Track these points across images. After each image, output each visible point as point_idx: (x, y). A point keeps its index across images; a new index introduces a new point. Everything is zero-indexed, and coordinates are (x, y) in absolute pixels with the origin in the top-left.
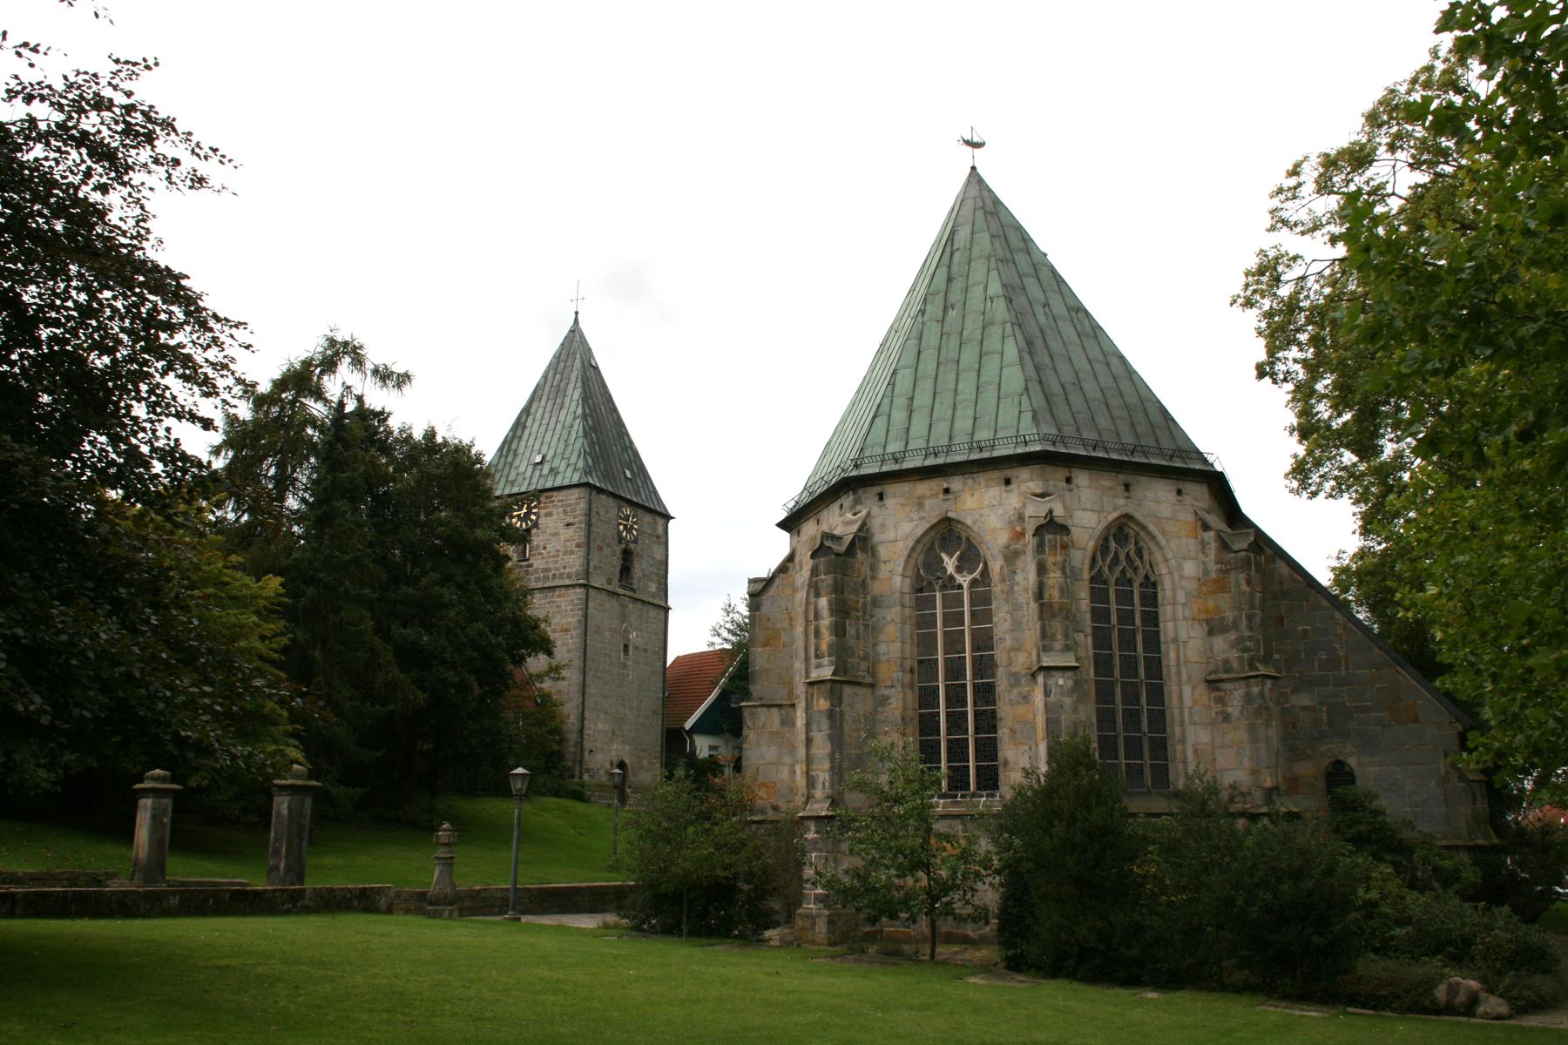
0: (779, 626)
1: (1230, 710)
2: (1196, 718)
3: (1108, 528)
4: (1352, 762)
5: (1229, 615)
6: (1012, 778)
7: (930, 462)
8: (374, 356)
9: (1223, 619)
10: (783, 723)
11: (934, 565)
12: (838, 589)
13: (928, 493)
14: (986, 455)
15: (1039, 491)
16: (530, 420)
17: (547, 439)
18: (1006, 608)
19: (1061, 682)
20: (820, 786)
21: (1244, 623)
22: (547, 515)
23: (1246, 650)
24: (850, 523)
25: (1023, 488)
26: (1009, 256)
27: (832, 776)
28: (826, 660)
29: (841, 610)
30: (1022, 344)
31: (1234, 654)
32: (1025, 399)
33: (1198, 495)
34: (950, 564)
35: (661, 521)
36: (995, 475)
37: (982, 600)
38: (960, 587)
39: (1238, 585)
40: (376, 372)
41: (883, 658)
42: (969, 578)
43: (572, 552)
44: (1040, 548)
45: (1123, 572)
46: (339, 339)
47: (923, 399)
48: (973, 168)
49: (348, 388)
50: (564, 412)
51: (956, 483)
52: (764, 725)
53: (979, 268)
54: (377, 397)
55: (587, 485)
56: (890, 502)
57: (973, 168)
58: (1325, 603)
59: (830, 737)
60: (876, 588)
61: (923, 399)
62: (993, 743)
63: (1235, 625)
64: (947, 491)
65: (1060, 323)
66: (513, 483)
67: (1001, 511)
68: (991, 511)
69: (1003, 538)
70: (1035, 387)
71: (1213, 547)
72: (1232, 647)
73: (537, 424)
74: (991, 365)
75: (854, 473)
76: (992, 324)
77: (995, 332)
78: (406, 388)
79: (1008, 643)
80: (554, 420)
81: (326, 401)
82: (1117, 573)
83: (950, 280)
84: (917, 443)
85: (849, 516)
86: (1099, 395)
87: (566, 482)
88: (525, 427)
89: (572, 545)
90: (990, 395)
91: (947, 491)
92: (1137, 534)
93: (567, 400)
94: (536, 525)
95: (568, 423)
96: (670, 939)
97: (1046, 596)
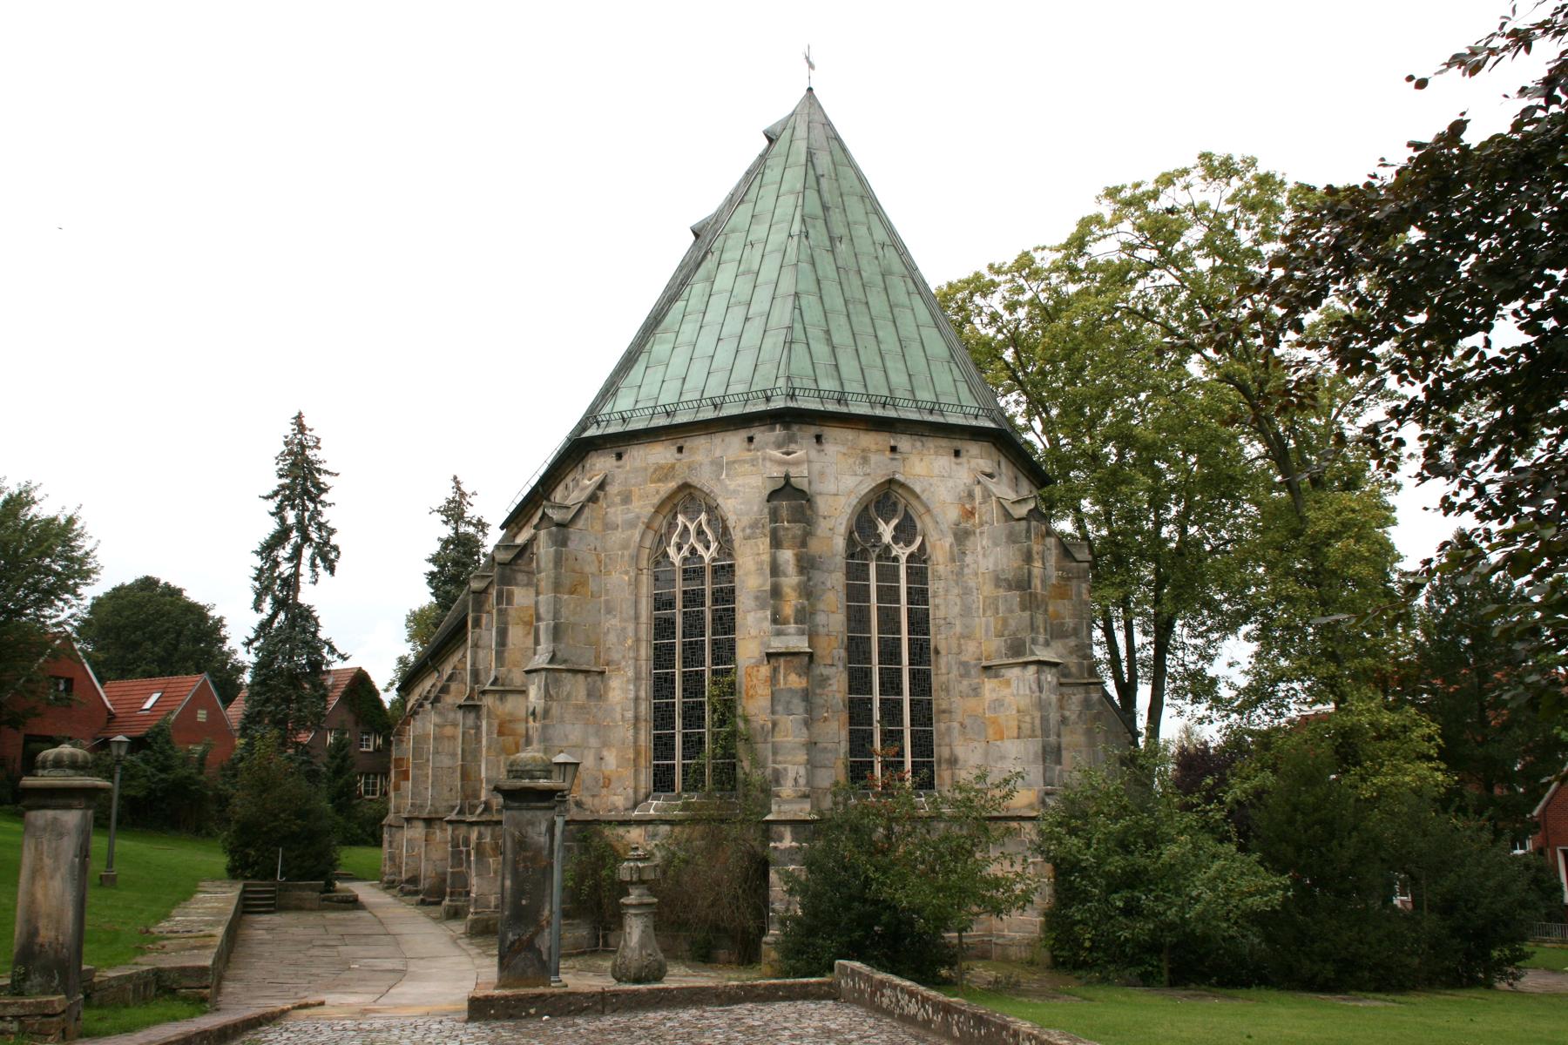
0: (588, 569)
1: (1067, 713)
9: (1062, 624)
10: (589, 695)
13: (873, 447)
15: (988, 470)
18: (956, 591)
20: (790, 782)
25: (974, 462)
34: (887, 531)
36: (944, 443)
37: (918, 574)
39: (1079, 594)
41: (822, 630)
42: (908, 551)
48: (810, 90)
51: (904, 443)
52: (569, 695)
56: (831, 448)
57: (810, 90)
61: (841, 336)
67: (950, 483)
69: (953, 514)
72: (1071, 653)
79: (958, 629)
82: (685, 552)
91: (893, 449)
96: (1464, 995)
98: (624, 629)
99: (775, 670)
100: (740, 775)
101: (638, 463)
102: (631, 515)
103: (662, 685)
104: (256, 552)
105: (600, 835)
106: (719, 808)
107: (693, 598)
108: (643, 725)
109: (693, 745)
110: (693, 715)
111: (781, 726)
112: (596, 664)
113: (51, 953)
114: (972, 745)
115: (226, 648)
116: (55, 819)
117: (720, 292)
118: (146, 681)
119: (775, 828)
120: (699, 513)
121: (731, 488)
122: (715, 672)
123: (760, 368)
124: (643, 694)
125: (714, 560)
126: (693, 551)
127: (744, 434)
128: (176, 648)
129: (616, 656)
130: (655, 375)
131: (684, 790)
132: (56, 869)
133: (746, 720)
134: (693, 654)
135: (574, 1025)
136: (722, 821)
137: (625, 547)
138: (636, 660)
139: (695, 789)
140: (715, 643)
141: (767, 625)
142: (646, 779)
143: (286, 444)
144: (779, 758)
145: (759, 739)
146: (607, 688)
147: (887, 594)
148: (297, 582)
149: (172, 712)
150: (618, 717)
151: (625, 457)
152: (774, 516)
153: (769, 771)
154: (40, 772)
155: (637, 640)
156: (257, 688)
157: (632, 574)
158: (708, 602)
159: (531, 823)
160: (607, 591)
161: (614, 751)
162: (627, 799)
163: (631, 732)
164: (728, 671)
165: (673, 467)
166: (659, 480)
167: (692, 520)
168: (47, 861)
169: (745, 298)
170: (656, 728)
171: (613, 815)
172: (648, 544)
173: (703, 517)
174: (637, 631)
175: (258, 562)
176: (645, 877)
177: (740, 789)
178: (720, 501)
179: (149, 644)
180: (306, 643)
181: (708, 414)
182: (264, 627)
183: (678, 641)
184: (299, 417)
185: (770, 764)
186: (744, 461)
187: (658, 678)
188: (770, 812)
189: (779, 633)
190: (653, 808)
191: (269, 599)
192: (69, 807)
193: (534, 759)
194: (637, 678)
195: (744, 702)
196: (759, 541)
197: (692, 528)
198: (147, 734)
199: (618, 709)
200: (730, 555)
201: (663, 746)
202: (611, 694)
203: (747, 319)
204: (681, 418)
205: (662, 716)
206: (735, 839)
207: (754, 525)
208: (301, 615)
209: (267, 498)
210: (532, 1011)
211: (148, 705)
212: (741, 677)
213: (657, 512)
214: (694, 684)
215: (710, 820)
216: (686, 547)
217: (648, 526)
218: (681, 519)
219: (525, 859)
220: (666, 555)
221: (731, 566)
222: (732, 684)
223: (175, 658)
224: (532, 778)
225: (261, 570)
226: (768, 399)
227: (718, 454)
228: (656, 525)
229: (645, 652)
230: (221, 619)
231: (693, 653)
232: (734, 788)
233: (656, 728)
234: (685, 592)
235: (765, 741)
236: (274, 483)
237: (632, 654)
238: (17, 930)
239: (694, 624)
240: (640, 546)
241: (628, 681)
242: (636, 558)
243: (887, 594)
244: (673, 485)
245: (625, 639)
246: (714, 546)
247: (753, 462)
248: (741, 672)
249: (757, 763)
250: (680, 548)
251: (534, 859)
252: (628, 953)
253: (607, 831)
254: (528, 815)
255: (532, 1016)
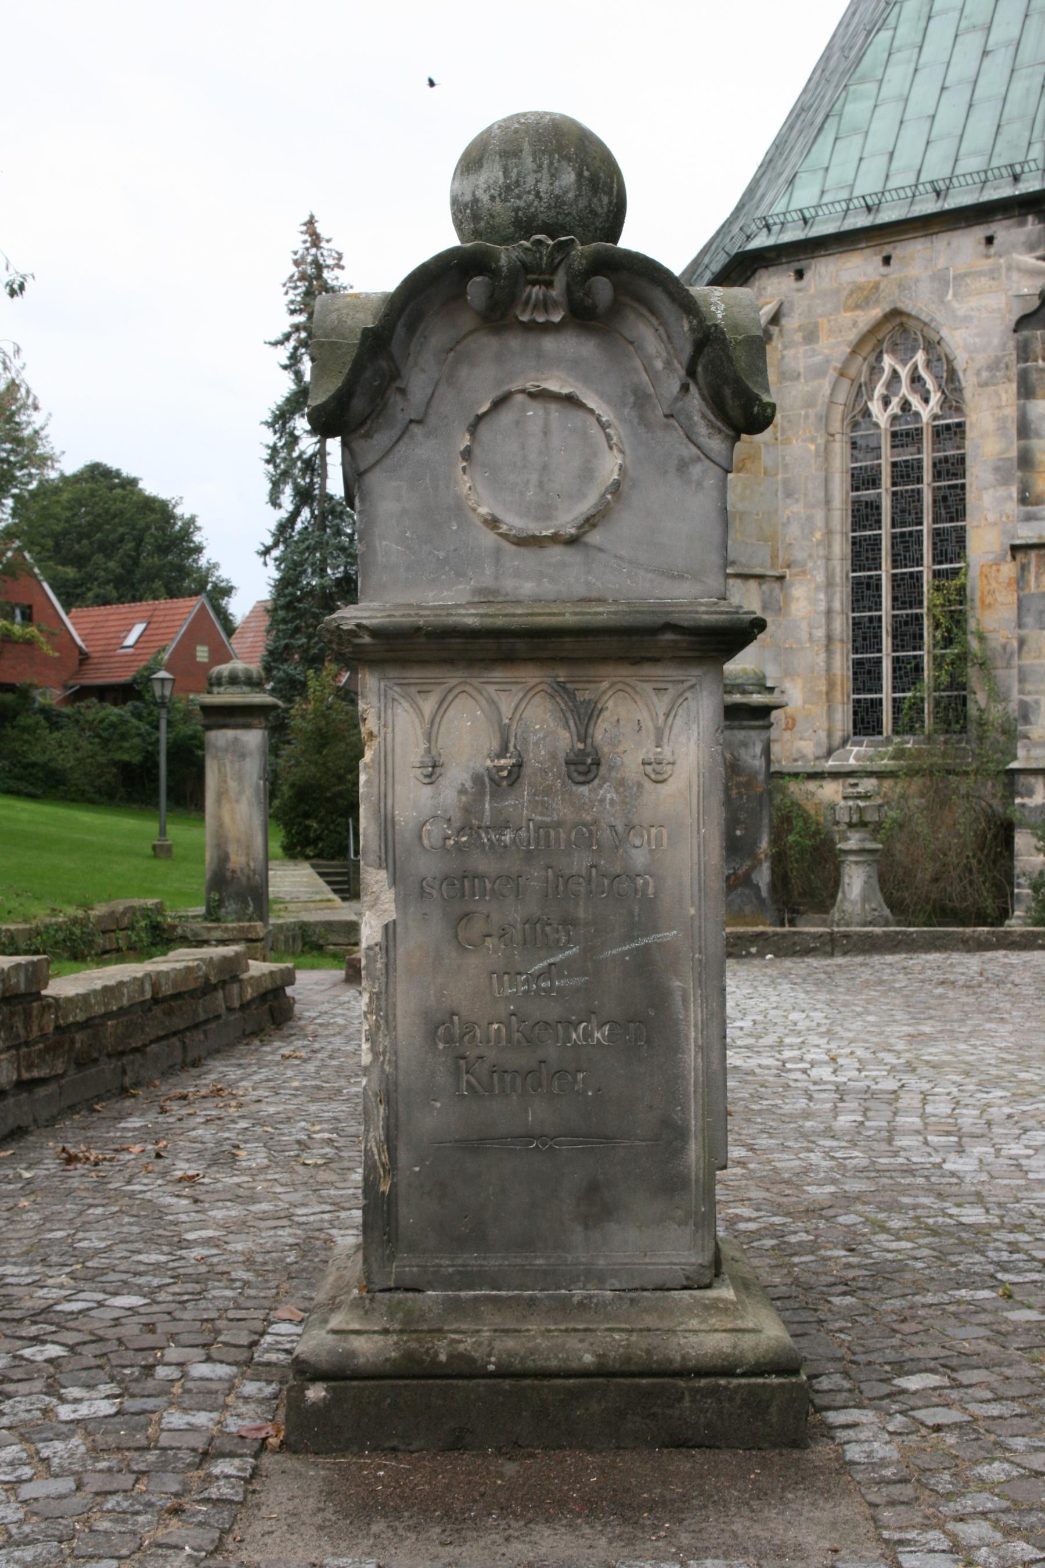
82: (894, 407)
98: (810, 518)
99: (1024, 568)
100: (972, 711)
101: (826, 284)
102: (819, 359)
103: (864, 593)
104: (266, 423)
105: (783, 790)
106: (944, 754)
107: (906, 472)
108: (837, 647)
109: (907, 673)
110: (907, 633)
111: (1031, 644)
112: (773, 566)
113: (244, 880)
115: (203, 562)
116: (236, 740)
117: (945, 12)
118: (124, 608)
119: (1022, 779)
120: (914, 351)
121: (961, 313)
122: (937, 574)
123: (1004, 130)
124: (837, 605)
125: (936, 417)
126: (906, 406)
127: (980, 232)
128: (136, 562)
129: (799, 555)
130: (850, 148)
131: (896, 732)
132: (241, 792)
133: (982, 638)
134: (907, 549)
135: (559, 1360)
136: (949, 772)
137: (809, 402)
138: (828, 559)
139: (911, 730)
140: (937, 533)
141: (1012, 507)
142: (843, 719)
143: (297, 263)
144: (1029, 687)
145: (999, 663)
146: (788, 599)
148: (324, 465)
149: (164, 649)
150: (804, 636)
151: (808, 276)
152: (1024, 352)
153: (1013, 706)
154: (215, 689)
155: (829, 532)
156: (281, 613)
157: (821, 441)
158: (927, 475)
159: (745, 744)
160: (786, 466)
161: (799, 682)
162: (818, 744)
163: (823, 656)
164: (956, 572)
165: (876, 287)
166: (857, 307)
167: (904, 363)
168: (232, 784)
169: (982, 19)
170: (856, 650)
171: (799, 766)
172: (841, 397)
173: (920, 357)
174: (827, 521)
175: (270, 437)
176: (867, 818)
177: (973, 731)
178: (944, 333)
179: (99, 558)
180: (343, 549)
181: (928, 206)
182: (284, 528)
183: (885, 532)
184: (311, 222)
185: (1015, 696)
186: (981, 274)
187: (857, 583)
188: (1015, 758)
189: (1029, 518)
190: (854, 756)
191: (288, 490)
192: (247, 726)
193: (745, 671)
194: (829, 584)
195: (978, 612)
196: (1001, 388)
197: (904, 373)
198: (135, 680)
199: (804, 625)
200: (959, 410)
201: (865, 675)
202: (794, 607)
203: (985, 53)
204: (887, 216)
205: (865, 635)
206: (967, 796)
207: (994, 366)
208: (332, 512)
209: (275, 344)
210: (753, 950)
211: (131, 640)
212: (974, 580)
213: (854, 352)
214: (907, 590)
215: (929, 773)
216: (895, 401)
217: (842, 374)
218: (888, 361)
219: (738, 785)
220: (867, 413)
221: (960, 425)
222: (962, 590)
223: (138, 575)
224: (744, 692)
225: (274, 449)
226: (1016, 178)
227: (941, 263)
228: (852, 372)
229: (840, 548)
230: (192, 520)
231: (906, 548)
232: (964, 730)
233: (856, 650)
234: (894, 465)
235: (1008, 666)
236: (286, 322)
237: (821, 552)
238: (208, 856)
239: (907, 509)
240: (831, 402)
241: (817, 588)
242: (825, 419)
244: (876, 313)
245: (812, 533)
246: (935, 397)
247: (993, 274)
248: (974, 572)
249: (997, 695)
250: (886, 402)
251: (748, 785)
252: (847, 906)
253: (794, 787)
254: (741, 735)
255: (753, 956)
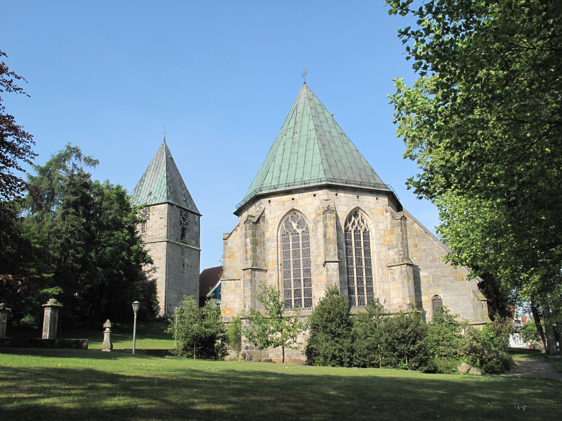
0: (234, 250)
1: (395, 277)
2: (383, 280)
3: (351, 212)
4: (441, 295)
5: (395, 243)
6: (316, 303)
7: (287, 188)
8: (85, 153)
11: (288, 226)
12: (254, 235)
14: (307, 186)
15: (326, 199)
16: (146, 178)
17: (153, 186)
18: (314, 241)
19: (333, 267)
21: (400, 245)
22: (152, 215)
23: (400, 255)
24: (259, 211)
25: (320, 197)
26: (317, 115)
27: (251, 303)
28: (249, 261)
29: (255, 243)
30: (321, 146)
31: (397, 256)
32: (321, 166)
33: (384, 200)
34: (295, 225)
35: (197, 217)
37: (306, 238)
38: (298, 234)
39: (398, 232)
40: (85, 160)
43: (162, 229)
44: (325, 219)
45: (357, 228)
46: (72, 147)
47: (285, 167)
49: (74, 165)
50: (159, 175)
51: (296, 196)
52: (229, 287)
53: (306, 119)
54: (87, 169)
55: (169, 203)
58: (431, 239)
59: (251, 289)
60: (267, 235)
62: (310, 290)
63: (397, 246)
64: (293, 199)
65: (335, 139)
66: (139, 202)
67: (312, 206)
68: (309, 204)
70: (325, 162)
71: (389, 218)
72: (396, 254)
73: (149, 180)
74: (310, 154)
75: (260, 193)
76: (310, 139)
77: (312, 142)
78: (97, 166)
79: (315, 254)
80: (155, 178)
81: (67, 171)
82: (354, 227)
83: (295, 123)
84: (283, 181)
85: (258, 209)
86: (349, 164)
87: (160, 202)
88: (144, 181)
89: (162, 226)
90: (309, 165)
92: (362, 214)
93: (160, 171)
94: (148, 218)
95: (161, 180)
97: (328, 236)
114: (320, 292)
147: (296, 245)
243: (296, 245)
